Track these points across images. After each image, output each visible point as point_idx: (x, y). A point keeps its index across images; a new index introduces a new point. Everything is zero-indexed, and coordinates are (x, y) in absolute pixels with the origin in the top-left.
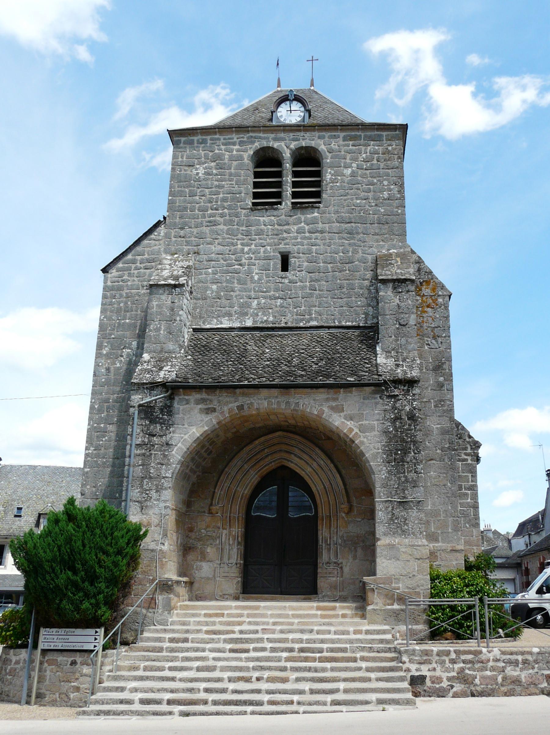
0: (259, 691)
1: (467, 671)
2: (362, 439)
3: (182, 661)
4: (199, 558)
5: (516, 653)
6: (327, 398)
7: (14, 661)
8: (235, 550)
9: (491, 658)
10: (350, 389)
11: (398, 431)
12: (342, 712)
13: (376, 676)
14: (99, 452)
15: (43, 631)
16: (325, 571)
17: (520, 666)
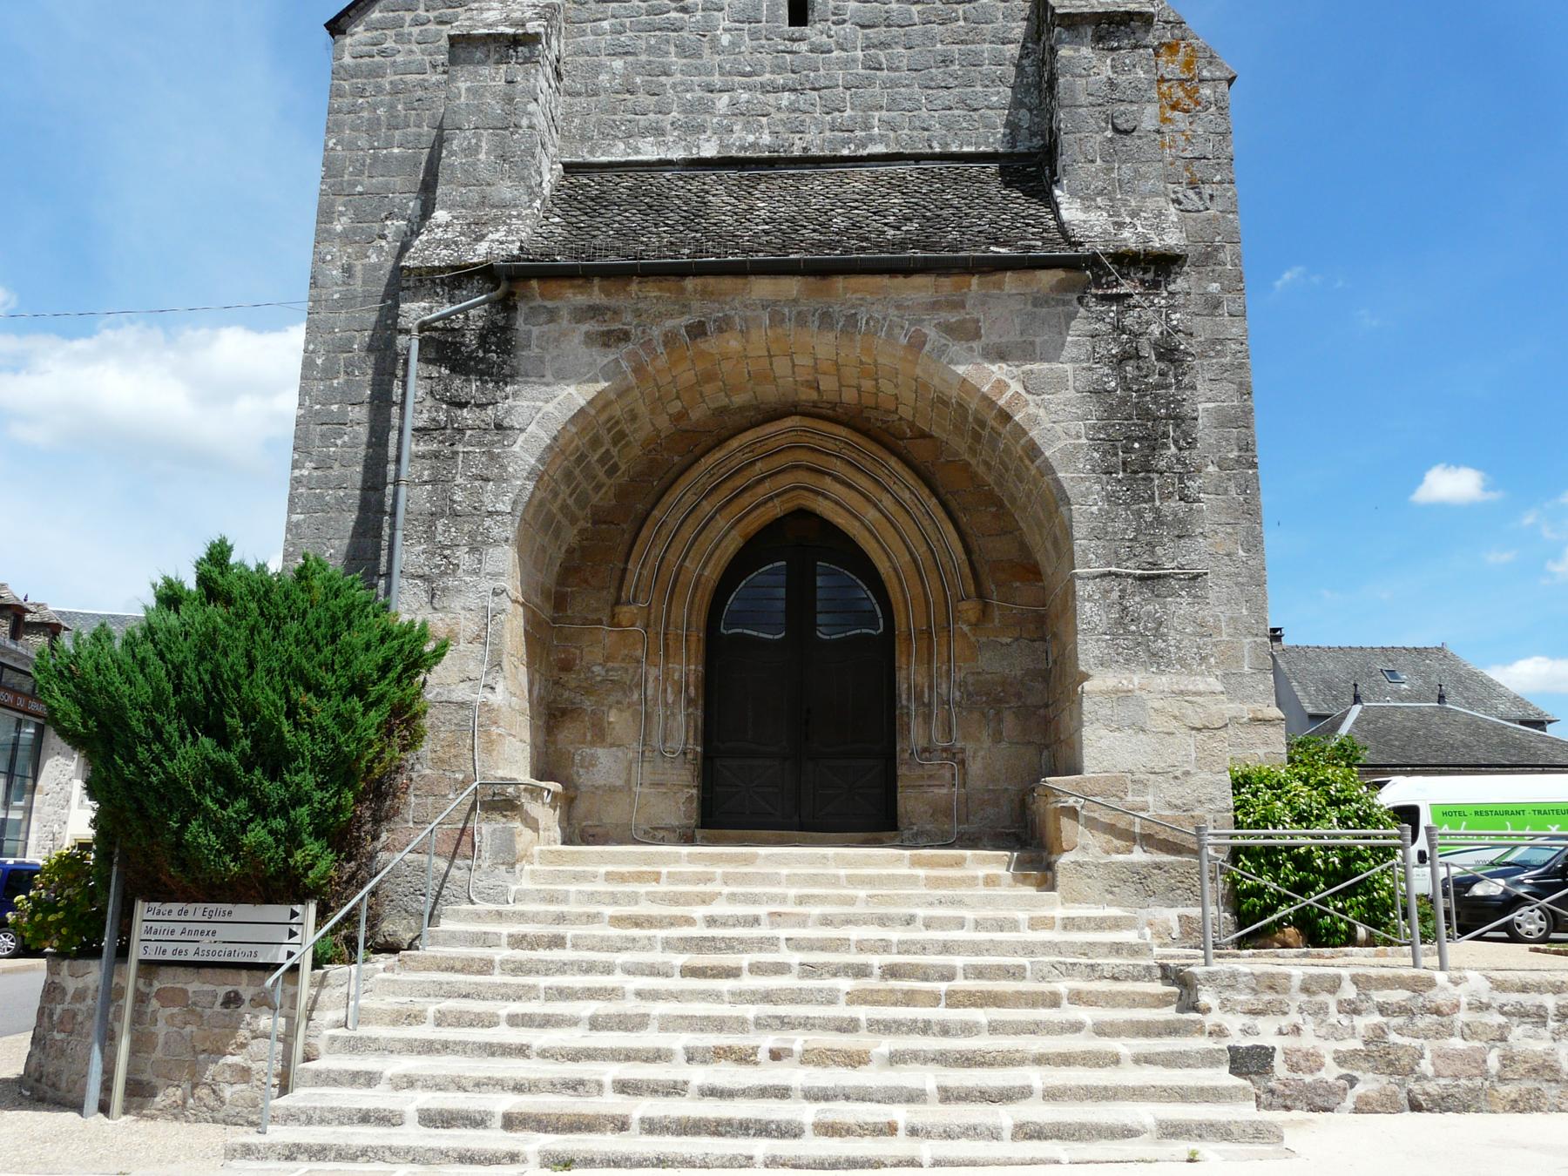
0: (782, 1093)
1: (1393, 1037)
2: (1032, 409)
3: (547, 1000)
4: (589, 738)
5: (1539, 988)
6: (935, 303)
7: (71, 991)
8: (681, 718)
9: (1464, 1000)
10: (996, 277)
11: (1130, 389)
12: (1058, 1162)
13: (1135, 1050)
14: (327, 472)
15: (142, 909)
16: (919, 772)
17: (1552, 1024)
